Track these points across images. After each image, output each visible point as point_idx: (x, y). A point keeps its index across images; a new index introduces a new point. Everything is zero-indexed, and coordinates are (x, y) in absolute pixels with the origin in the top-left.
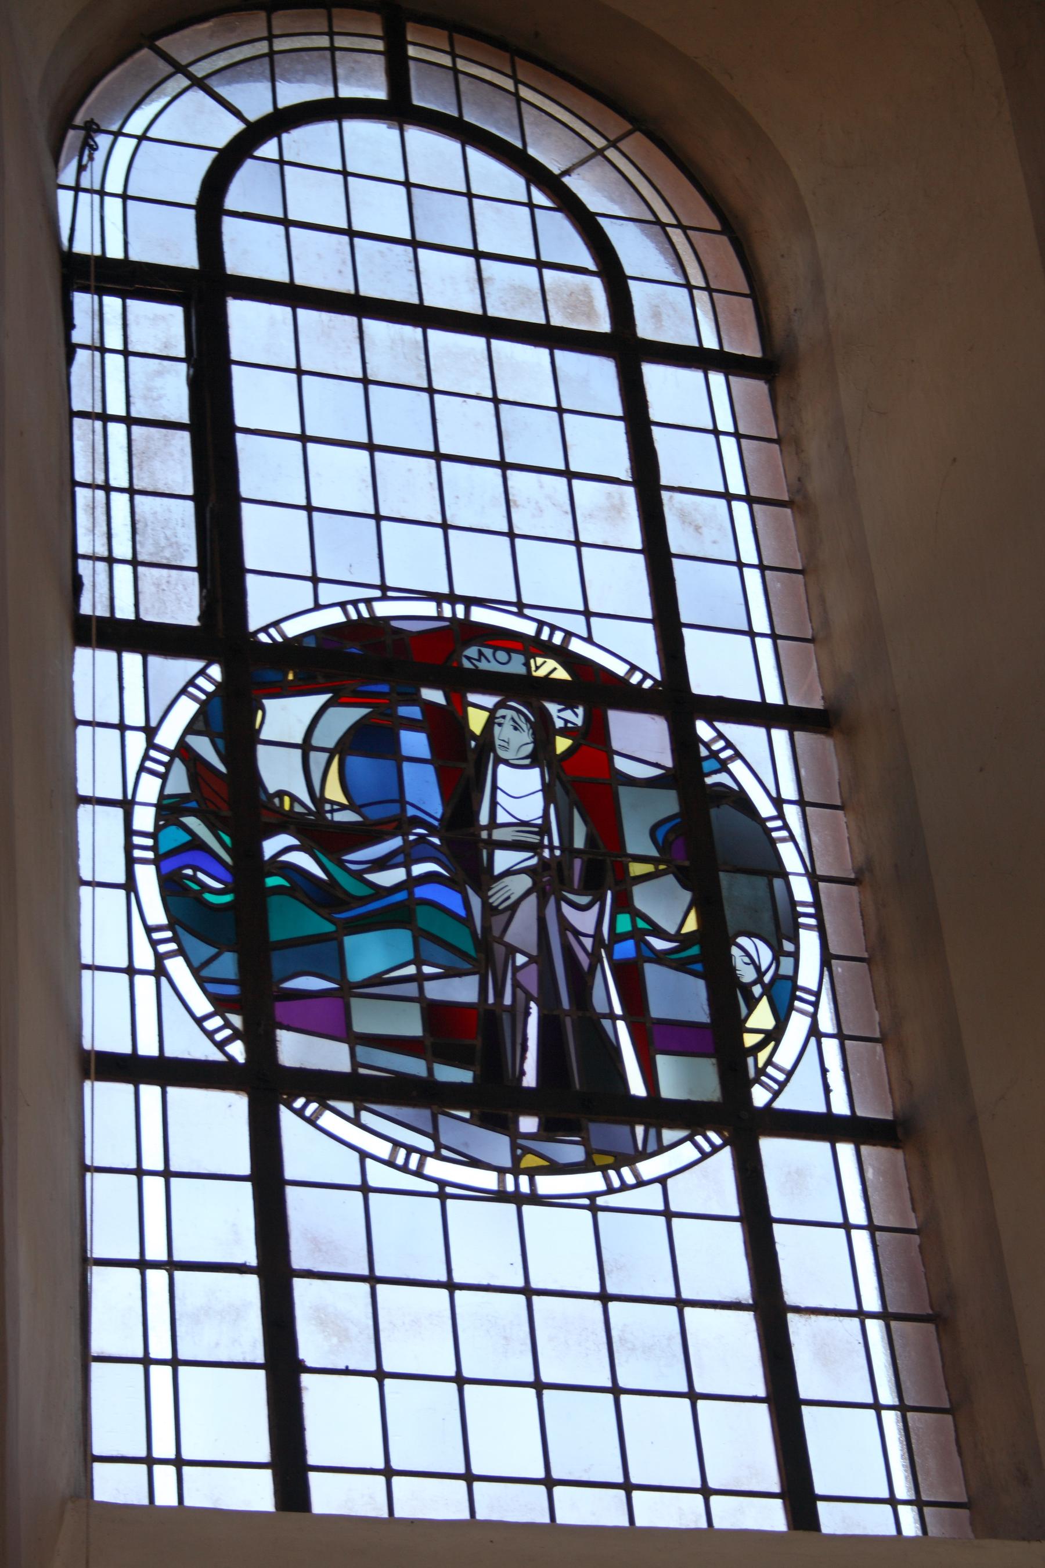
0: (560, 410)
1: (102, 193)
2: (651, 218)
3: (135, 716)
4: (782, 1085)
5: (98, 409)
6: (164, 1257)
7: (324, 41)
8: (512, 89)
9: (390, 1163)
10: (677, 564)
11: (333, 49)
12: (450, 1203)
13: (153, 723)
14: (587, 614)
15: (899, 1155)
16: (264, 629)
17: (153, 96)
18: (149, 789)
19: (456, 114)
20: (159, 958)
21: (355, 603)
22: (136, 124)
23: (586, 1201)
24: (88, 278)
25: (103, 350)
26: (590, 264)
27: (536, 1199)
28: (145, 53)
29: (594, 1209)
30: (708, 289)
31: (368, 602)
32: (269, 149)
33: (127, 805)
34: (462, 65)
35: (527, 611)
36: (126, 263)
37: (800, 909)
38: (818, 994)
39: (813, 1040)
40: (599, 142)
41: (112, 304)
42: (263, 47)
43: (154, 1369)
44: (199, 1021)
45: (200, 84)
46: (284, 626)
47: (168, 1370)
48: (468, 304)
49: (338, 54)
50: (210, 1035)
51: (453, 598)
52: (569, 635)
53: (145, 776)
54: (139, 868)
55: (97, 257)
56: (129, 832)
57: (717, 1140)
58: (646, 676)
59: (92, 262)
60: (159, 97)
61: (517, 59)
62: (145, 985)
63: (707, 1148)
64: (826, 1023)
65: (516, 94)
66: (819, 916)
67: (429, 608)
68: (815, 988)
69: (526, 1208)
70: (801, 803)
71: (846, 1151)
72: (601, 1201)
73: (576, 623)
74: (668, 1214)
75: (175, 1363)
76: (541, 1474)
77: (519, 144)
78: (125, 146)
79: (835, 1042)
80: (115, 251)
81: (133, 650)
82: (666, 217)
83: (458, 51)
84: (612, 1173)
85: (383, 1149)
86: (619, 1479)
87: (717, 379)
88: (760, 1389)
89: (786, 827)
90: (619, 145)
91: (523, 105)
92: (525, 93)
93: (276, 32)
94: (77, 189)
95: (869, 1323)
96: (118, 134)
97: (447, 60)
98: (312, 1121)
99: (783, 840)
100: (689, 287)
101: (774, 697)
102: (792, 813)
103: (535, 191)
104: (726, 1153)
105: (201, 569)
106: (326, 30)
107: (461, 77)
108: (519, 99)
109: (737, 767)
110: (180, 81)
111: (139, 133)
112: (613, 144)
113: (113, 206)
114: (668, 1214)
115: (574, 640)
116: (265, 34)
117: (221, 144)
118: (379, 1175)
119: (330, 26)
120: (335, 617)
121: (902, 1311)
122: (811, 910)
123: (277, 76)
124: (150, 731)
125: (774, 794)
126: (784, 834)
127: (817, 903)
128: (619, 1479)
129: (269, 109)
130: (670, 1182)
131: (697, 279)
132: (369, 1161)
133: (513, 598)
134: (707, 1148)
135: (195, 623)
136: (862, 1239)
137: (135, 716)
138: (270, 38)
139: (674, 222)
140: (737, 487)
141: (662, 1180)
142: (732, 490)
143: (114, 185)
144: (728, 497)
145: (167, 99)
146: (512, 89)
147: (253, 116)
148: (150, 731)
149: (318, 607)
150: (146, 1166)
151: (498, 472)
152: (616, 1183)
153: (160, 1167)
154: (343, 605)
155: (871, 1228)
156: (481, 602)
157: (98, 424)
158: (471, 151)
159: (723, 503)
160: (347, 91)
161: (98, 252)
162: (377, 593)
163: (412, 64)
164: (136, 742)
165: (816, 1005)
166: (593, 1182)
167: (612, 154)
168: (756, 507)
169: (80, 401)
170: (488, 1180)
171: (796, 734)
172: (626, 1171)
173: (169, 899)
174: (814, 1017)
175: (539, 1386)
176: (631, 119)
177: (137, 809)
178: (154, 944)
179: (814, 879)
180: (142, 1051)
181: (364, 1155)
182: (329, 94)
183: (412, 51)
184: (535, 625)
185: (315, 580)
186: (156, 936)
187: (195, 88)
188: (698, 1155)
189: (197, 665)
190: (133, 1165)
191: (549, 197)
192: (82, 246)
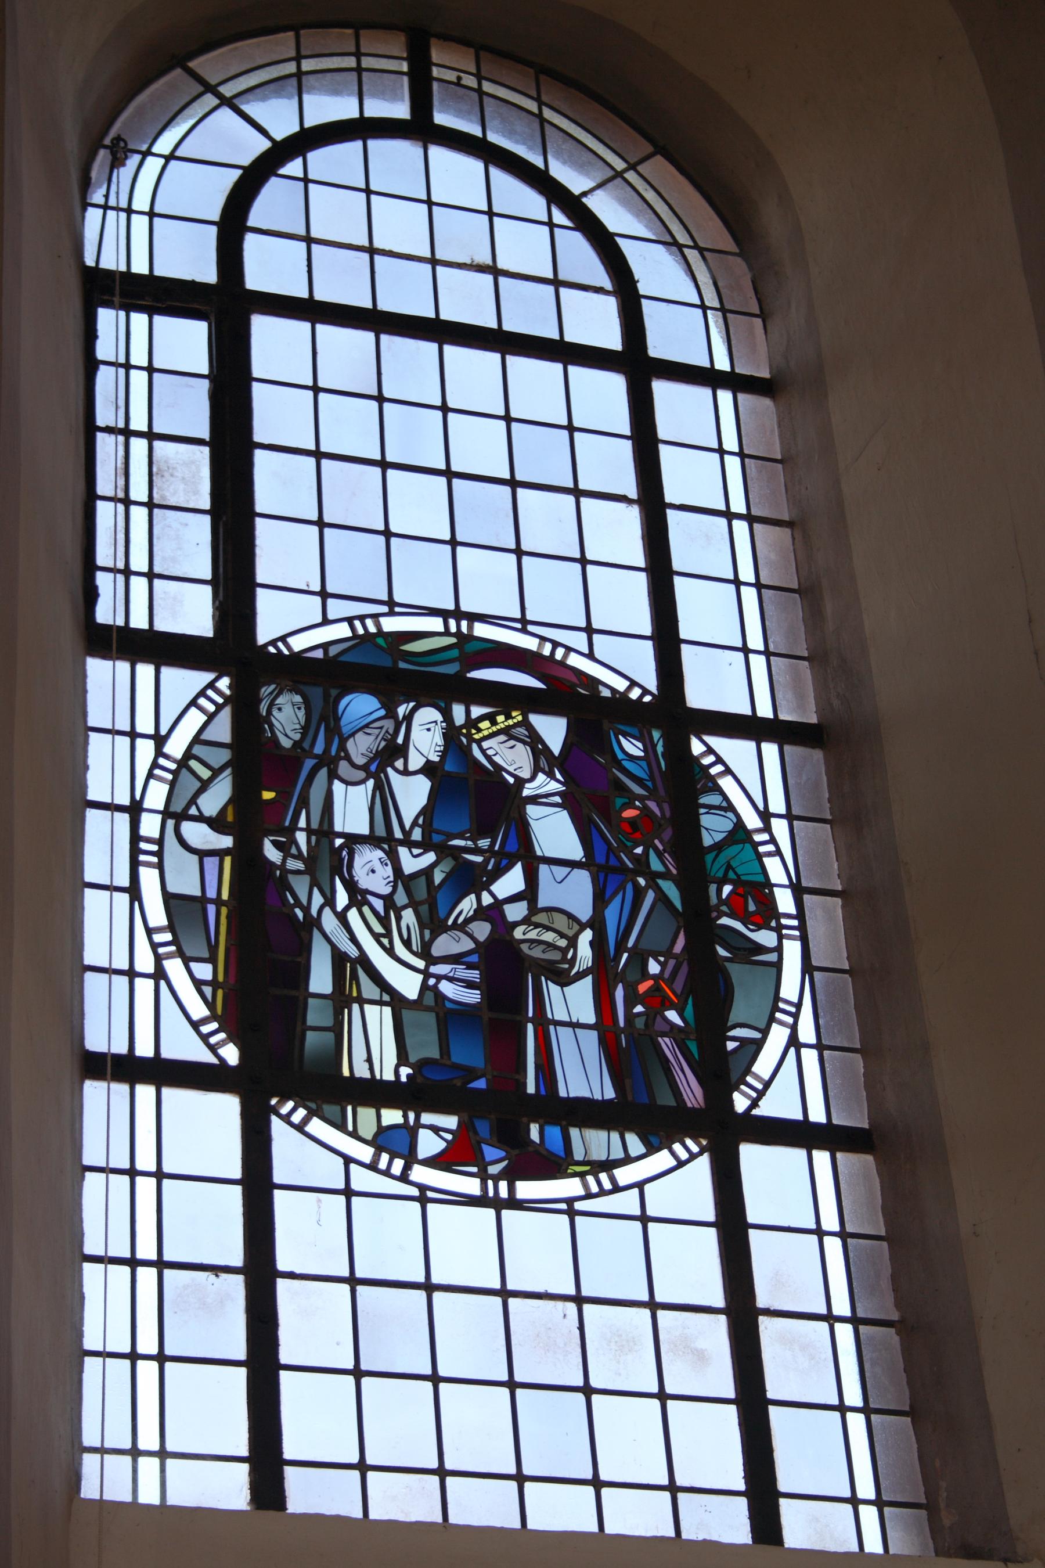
0: (571, 428)
1: (129, 211)
2: (670, 240)
3: (145, 724)
5: (121, 424)
6: (154, 1257)
7: (351, 62)
8: (536, 110)
10: (677, 580)
11: (359, 70)
13: (163, 732)
14: (589, 630)
15: (869, 1158)
18: (156, 796)
19: (480, 134)
21: (362, 618)
22: (164, 144)
24: (113, 295)
25: (128, 366)
26: (608, 285)
28: (178, 71)
29: (572, 1213)
31: (375, 617)
32: (294, 167)
33: (135, 809)
34: (487, 87)
35: (530, 628)
36: (151, 280)
37: (797, 933)
38: (799, 1006)
39: (792, 1050)
40: (619, 165)
41: (139, 320)
42: (291, 68)
43: (141, 1364)
46: (290, 640)
47: (156, 1461)
51: (458, 614)
54: (143, 871)
55: (121, 273)
56: (135, 838)
57: (695, 1149)
59: (118, 277)
62: (144, 988)
64: (807, 1033)
65: (540, 116)
66: (802, 928)
67: (436, 624)
69: (505, 1213)
70: (789, 817)
71: (822, 1158)
74: (644, 1219)
76: (512, 1470)
78: (153, 165)
79: (814, 1053)
80: (140, 267)
81: (146, 660)
82: (682, 238)
84: (590, 1179)
87: (725, 397)
88: (729, 1391)
89: (773, 841)
90: (639, 168)
91: (547, 126)
94: (106, 207)
99: (769, 854)
100: (703, 307)
101: (765, 710)
102: (780, 828)
105: (214, 582)
106: (353, 49)
107: (486, 99)
108: (542, 121)
110: (210, 100)
111: (167, 152)
112: (632, 167)
113: (140, 223)
114: (644, 1219)
119: (358, 45)
120: (342, 631)
121: (870, 1316)
123: (304, 89)
124: (160, 740)
125: (761, 807)
126: (771, 848)
127: (800, 915)
130: (647, 1187)
135: (209, 633)
136: (834, 1246)
137: (145, 724)
138: (298, 59)
139: (691, 243)
140: (738, 506)
142: (733, 509)
143: (141, 202)
144: (729, 515)
146: (536, 110)
147: (279, 135)
148: (160, 740)
149: (326, 621)
152: (594, 1189)
154: (350, 620)
155: (843, 1235)
156: (483, 618)
157: (121, 439)
158: (494, 171)
159: (723, 522)
160: (376, 108)
161: (123, 268)
162: (579, 1206)
163: (435, 86)
164: (146, 749)
165: (796, 1016)
166: (390, 624)
167: (631, 176)
168: (757, 526)
169: (104, 416)
172: (603, 1177)
174: (794, 1028)
175: (512, 1385)
176: (651, 141)
177: (145, 816)
179: (798, 890)
181: (348, 1160)
183: (435, 72)
185: (324, 594)
188: (674, 1163)
189: (209, 677)
191: (569, 218)
192: (108, 262)
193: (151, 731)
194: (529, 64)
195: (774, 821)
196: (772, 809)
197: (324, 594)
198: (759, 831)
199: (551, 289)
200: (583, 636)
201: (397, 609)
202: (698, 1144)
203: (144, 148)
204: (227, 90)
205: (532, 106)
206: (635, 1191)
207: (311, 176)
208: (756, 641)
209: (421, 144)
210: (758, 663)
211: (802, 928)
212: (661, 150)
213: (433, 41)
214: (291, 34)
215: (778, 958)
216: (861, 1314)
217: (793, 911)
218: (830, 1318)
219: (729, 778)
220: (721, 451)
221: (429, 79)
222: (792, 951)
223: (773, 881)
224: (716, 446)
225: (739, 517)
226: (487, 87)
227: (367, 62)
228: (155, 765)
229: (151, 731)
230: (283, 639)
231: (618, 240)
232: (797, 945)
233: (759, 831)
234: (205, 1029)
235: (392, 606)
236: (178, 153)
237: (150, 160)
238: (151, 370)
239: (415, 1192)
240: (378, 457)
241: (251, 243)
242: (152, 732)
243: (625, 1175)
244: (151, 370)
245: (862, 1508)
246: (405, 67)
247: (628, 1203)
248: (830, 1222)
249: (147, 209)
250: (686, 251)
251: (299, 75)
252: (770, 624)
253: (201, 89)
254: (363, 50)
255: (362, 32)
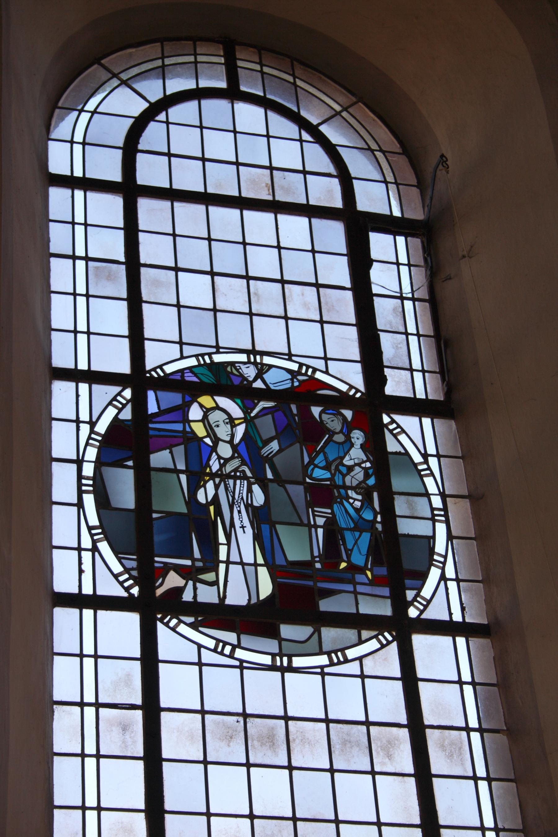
2: (366, 147)
3: (84, 416)
4: (426, 607)
7: (191, 59)
9: (215, 650)
11: (196, 63)
12: (245, 671)
14: (326, 359)
16: (154, 369)
17: (100, 90)
18: (92, 454)
20: (94, 542)
21: (203, 355)
22: (91, 105)
23: (319, 670)
26: (334, 172)
27: (291, 669)
28: (96, 66)
29: (323, 674)
30: (396, 183)
31: (210, 355)
32: (162, 117)
33: (79, 462)
34: (266, 69)
35: (294, 358)
42: (159, 63)
44: (116, 576)
45: (125, 83)
47: (95, 813)
48: (215, 211)
49: (199, 65)
50: (121, 583)
52: (315, 370)
53: (89, 448)
56: (80, 477)
57: (390, 638)
58: (357, 391)
60: (103, 92)
61: (295, 63)
62: (87, 556)
63: (384, 642)
64: (450, 573)
65: (294, 84)
66: (446, 515)
68: (444, 554)
69: (287, 675)
71: (461, 641)
72: (326, 670)
73: (320, 365)
74: (363, 676)
75: (98, 756)
77: (296, 110)
78: (85, 117)
82: (374, 146)
83: (264, 63)
85: (211, 643)
86: (333, 817)
89: (429, 468)
92: (299, 83)
93: (166, 55)
95: (472, 734)
96: (81, 111)
97: (258, 67)
98: (173, 629)
100: (386, 182)
101: (457, 617)
102: (433, 462)
103: (303, 133)
104: (394, 645)
106: (193, 53)
109: (403, 438)
111: (92, 109)
115: (318, 373)
116: (160, 56)
117: (136, 114)
118: (208, 657)
122: (442, 513)
124: (92, 424)
127: (445, 508)
128: (333, 817)
129: (161, 96)
131: (390, 178)
132: (202, 649)
133: (286, 351)
134: (384, 642)
136: (468, 690)
137: (84, 416)
141: (360, 659)
145: (107, 92)
147: (153, 100)
149: (182, 357)
150: (85, 652)
151: (314, 289)
153: (92, 653)
154: (196, 356)
158: (270, 113)
160: (204, 83)
164: (85, 429)
165: (444, 563)
167: (344, 114)
170: (267, 660)
171: (435, 420)
173: (101, 511)
174: (443, 570)
177: (85, 464)
178: (92, 535)
179: (443, 496)
180: (80, 367)
181: (200, 646)
182: (194, 86)
184: (297, 365)
186: (93, 532)
187: (123, 85)
189: (118, 389)
190: (78, 652)
193: (87, 419)
194: (288, 57)
195: (430, 459)
196: (429, 452)
197: (181, 343)
198: (421, 463)
199: (301, 176)
200: (323, 362)
201: (221, 350)
202: (391, 635)
203: (80, 108)
204: (124, 76)
205: (291, 79)
206: (357, 663)
207: (198, 130)
208: (403, 259)
209: (230, 101)
210: (404, 270)
211: (446, 515)
212: (361, 99)
213: (237, 47)
214: (158, 44)
215: (441, 582)
216: (484, 726)
217: (441, 506)
218: (467, 729)
219: (404, 435)
220: (398, 264)
221: (236, 67)
222: (441, 529)
223: (430, 492)
224: (395, 261)
225: (474, 730)
226: (266, 69)
227: (200, 58)
228: (89, 438)
229: (87, 419)
230: (161, 367)
231: (338, 148)
232: (444, 526)
233: (421, 463)
234: (121, 579)
235: (218, 349)
236: (98, 110)
237: (83, 114)
238: (86, 225)
239: (237, 663)
240: (208, 269)
241: (140, 158)
242: (88, 420)
243: (351, 653)
244: (86, 225)
245: (480, 782)
246: (222, 60)
247: (354, 668)
248: (466, 676)
249: (81, 141)
250: (376, 153)
251: (163, 66)
252: (390, 175)
253: (110, 76)
254: (198, 52)
255: (197, 43)
